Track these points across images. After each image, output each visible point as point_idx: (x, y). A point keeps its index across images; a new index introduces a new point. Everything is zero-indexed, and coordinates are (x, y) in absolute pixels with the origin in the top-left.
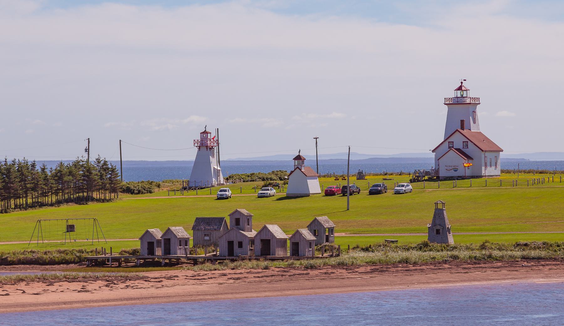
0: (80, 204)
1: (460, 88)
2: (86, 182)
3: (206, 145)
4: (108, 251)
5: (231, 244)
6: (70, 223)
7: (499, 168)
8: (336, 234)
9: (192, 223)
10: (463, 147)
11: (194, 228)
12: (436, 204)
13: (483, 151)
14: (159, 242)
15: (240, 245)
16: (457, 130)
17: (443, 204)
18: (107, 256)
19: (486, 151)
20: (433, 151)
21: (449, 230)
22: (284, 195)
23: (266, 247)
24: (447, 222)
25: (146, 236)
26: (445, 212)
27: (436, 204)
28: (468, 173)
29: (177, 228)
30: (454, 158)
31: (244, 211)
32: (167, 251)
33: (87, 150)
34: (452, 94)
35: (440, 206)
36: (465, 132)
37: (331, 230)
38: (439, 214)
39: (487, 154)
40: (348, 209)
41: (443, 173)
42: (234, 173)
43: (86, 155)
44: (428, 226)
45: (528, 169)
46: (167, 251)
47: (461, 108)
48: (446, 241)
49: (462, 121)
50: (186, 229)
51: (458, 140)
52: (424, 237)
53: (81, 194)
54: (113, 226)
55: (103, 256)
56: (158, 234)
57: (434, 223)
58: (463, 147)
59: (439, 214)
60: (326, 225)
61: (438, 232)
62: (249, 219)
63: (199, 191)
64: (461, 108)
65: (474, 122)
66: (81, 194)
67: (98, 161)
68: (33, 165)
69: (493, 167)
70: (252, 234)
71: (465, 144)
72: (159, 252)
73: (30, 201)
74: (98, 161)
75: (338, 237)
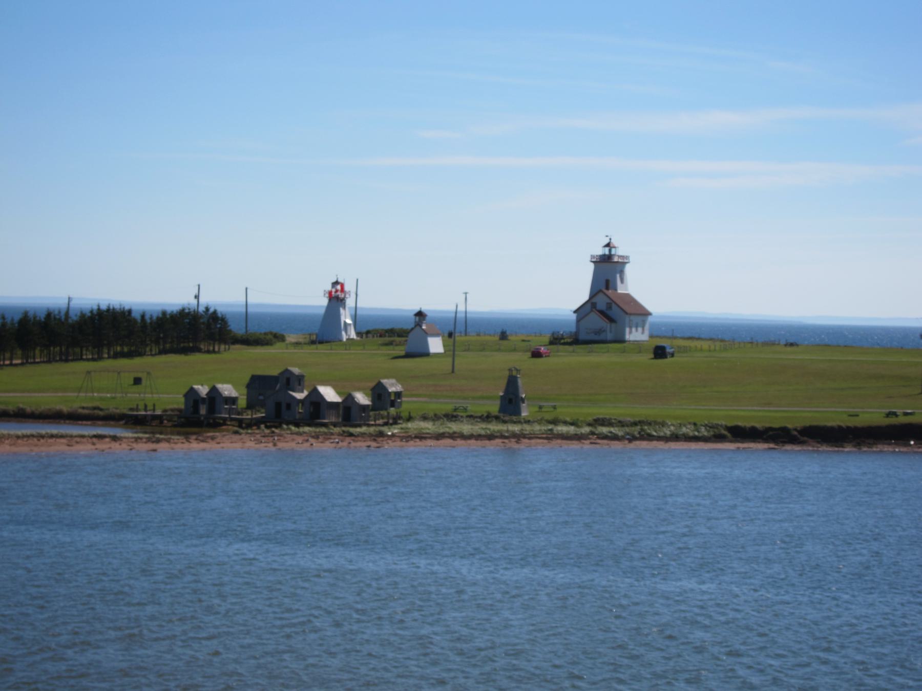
0: (185, 351)
1: (608, 245)
2: (193, 330)
3: (336, 299)
4: (141, 407)
5: (278, 405)
6: (139, 375)
7: (647, 333)
8: (404, 399)
9: (247, 379)
10: (607, 308)
11: (248, 386)
12: (510, 370)
13: (627, 313)
14: (204, 399)
15: (289, 406)
16: (600, 291)
17: (517, 370)
18: (149, 413)
19: (631, 314)
20: (575, 312)
21: (523, 400)
22: (403, 353)
23: (316, 409)
24: (521, 390)
25: (191, 394)
26: (520, 382)
27: (510, 370)
28: (610, 336)
29: (225, 386)
30: (596, 321)
31: (296, 370)
32: (212, 409)
33: (197, 297)
34: (600, 251)
35: (514, 373)
36: (610, 292)
37: (398, 395)
38: (512, 382)
39: (632, 317)
40: (453, 372)
41: (582, 337)
42: (370, 328)
43: (195, 302)
44: (501, 394)
45: (688, 335)
46: (212, 409)
47: (608, 267)
48: (517, 412)
49: (607, 282)
50: (235, 386)
51: (601, 302)
52: (494, 408)
53: (186, 345)
54: (169, 380)
55: (144, 413)
56: (203, 390)
57: (507, 391)
58: (607, 308)
59: (512, 382)
60: (392, 389)
61: (510, 401)
62: (300, 379)
63: (320, 346)
64: (608, 267)
65: (622, 281)
66: (186, 345)
67: (207, 309)
68: (60, 312)
69: (640, 329)
70: (300, 396)
71: (609, 306)
72: (203, 411)
73: (126, 349)
74: (207, 309)
75: (408, 402)
